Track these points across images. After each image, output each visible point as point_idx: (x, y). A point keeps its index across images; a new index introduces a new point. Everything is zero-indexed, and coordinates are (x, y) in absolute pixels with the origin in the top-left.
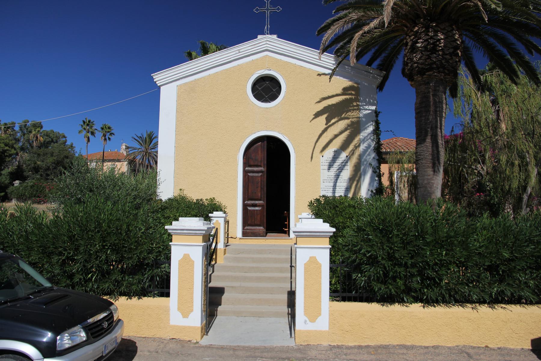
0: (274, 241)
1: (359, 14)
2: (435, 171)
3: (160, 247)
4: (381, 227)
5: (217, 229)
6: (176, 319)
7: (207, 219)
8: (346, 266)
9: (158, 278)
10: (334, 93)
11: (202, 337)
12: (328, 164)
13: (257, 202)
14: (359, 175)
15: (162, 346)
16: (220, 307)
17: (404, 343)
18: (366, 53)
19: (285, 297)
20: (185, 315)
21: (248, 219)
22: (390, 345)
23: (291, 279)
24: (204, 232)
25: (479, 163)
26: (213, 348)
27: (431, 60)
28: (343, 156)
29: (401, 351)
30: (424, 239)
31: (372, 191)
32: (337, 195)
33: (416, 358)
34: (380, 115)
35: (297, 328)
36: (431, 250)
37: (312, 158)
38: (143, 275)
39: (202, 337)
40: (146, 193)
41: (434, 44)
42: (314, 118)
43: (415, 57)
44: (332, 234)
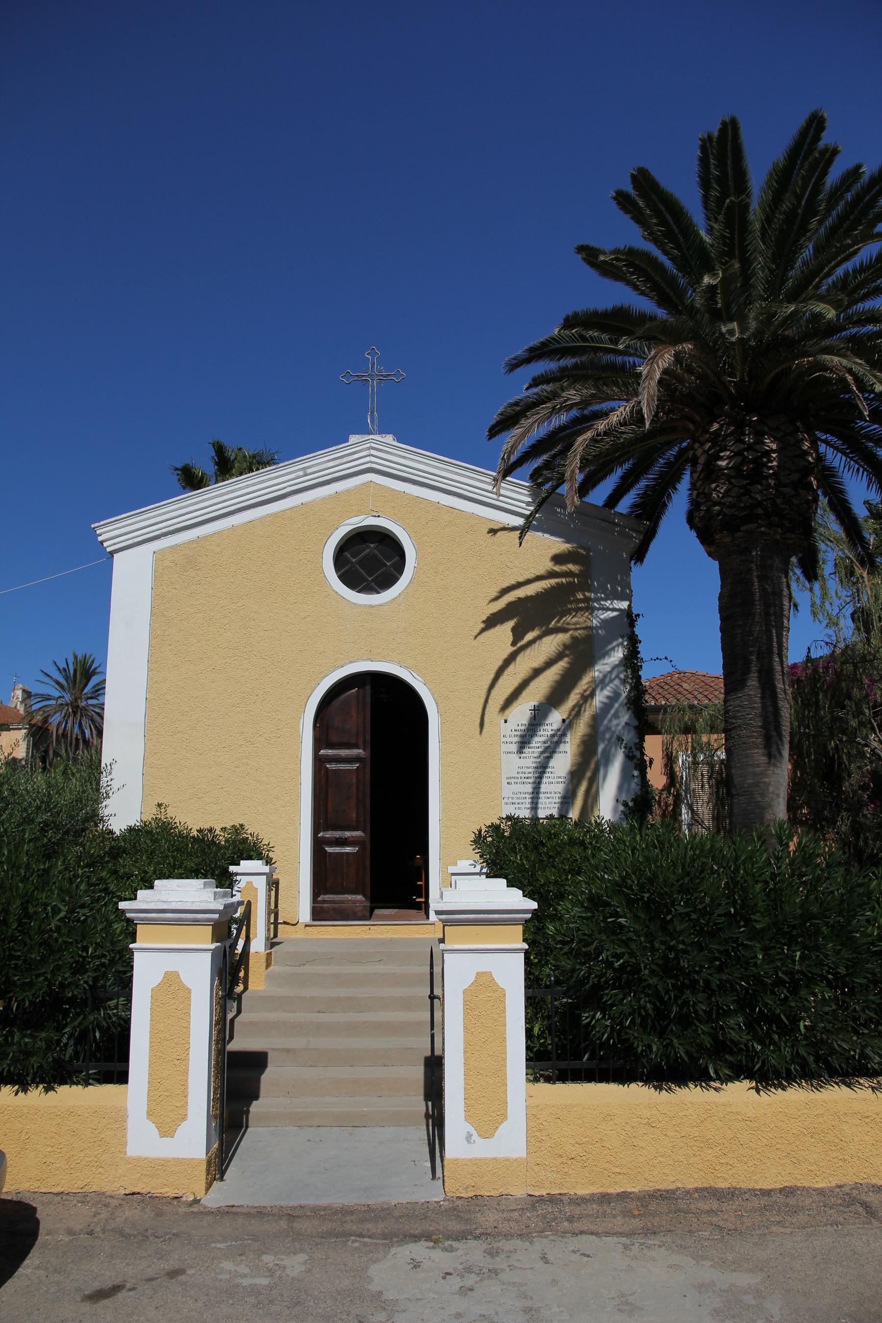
0: (389, 931)
1: (584, 391)
2: (772, 755)
3: (104, 956)
4: (647, 895)
5: (249, 903)
6: (143, 1140)
7: (225, 880)
8: (565, 994)
9: (97, 1035)
10: (531, 576)
11: (209, 1186)
12: (517, 739)
13: (348, 834)
14: (592, 766)
15: (104, 1214)
16: (254, 1102)
17: (713, 1184)
18: (604, 477)
19: (418, 1072)
20: (167, 1130)
21: (326, 874)
22: (678, 1189)
23: (432, 1028)
24: (217, 916)
25: (873, 729)
26: (236, 1214)
27: (750, 496)
28: (555, 719)
29: (704, 1205)
30: (748, 921)
31: (625, 804)
32: (542, 814)
33: (743, 1223)
34: (639, 623)
35: (449, 1153)
36: (765, 950)
37: (482, 725)
38: (59, 1029)
39: (209, 1186)
40: (72, 817)
41: (755, 461)
42: (483, 630)
43: (715, 490)
44: (529, 916)
